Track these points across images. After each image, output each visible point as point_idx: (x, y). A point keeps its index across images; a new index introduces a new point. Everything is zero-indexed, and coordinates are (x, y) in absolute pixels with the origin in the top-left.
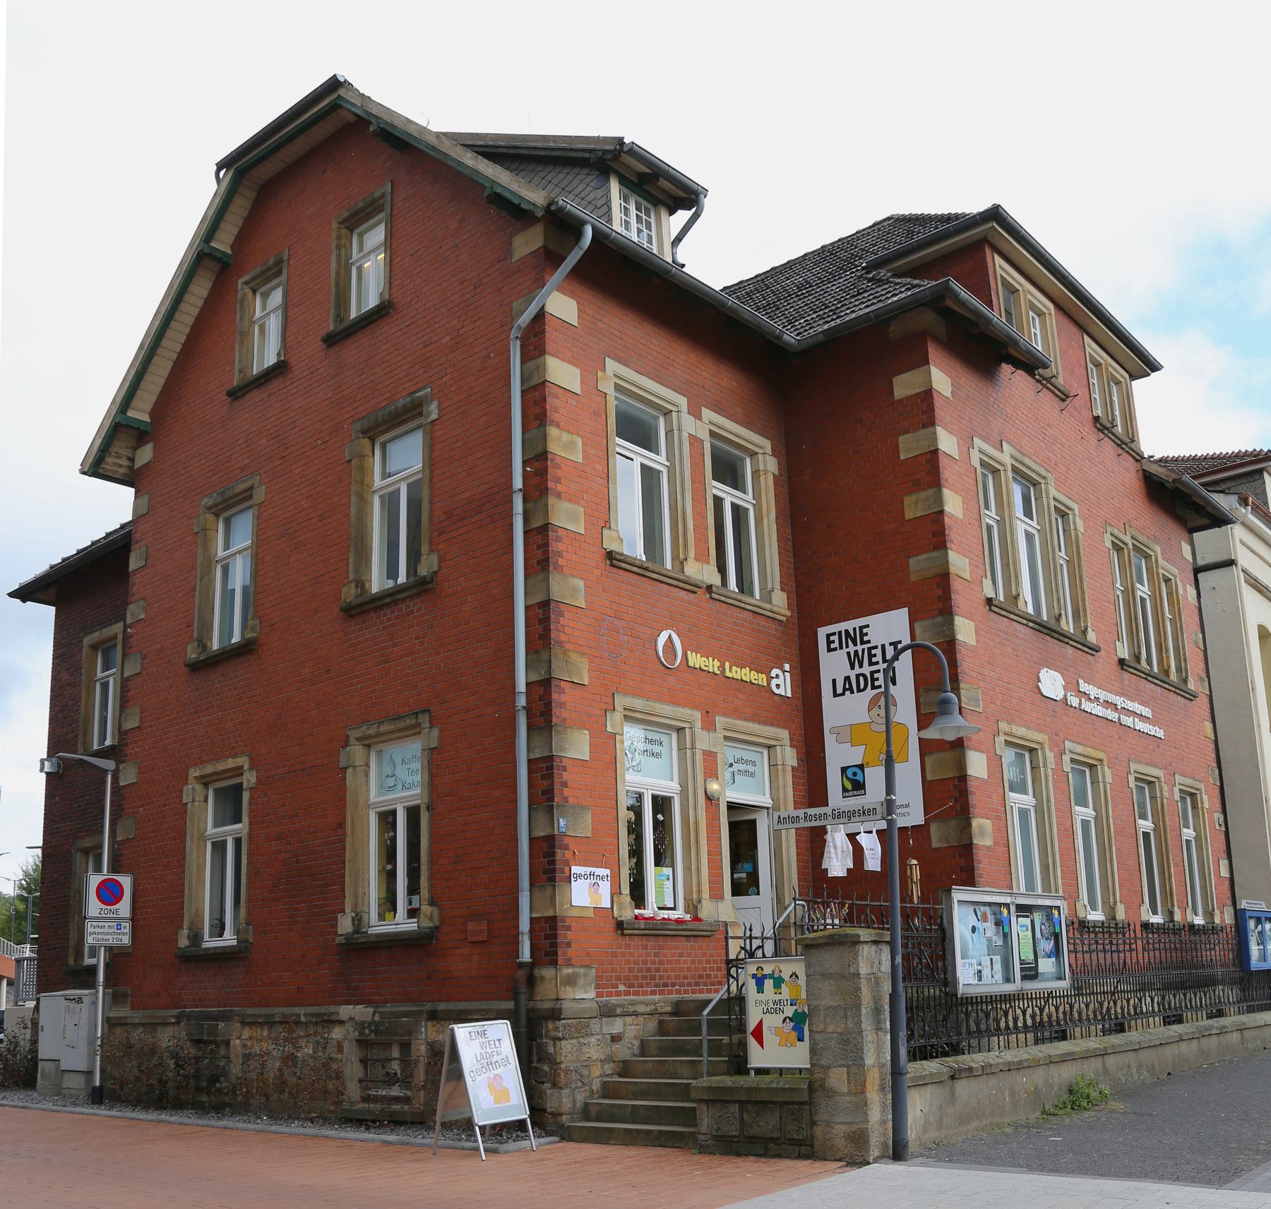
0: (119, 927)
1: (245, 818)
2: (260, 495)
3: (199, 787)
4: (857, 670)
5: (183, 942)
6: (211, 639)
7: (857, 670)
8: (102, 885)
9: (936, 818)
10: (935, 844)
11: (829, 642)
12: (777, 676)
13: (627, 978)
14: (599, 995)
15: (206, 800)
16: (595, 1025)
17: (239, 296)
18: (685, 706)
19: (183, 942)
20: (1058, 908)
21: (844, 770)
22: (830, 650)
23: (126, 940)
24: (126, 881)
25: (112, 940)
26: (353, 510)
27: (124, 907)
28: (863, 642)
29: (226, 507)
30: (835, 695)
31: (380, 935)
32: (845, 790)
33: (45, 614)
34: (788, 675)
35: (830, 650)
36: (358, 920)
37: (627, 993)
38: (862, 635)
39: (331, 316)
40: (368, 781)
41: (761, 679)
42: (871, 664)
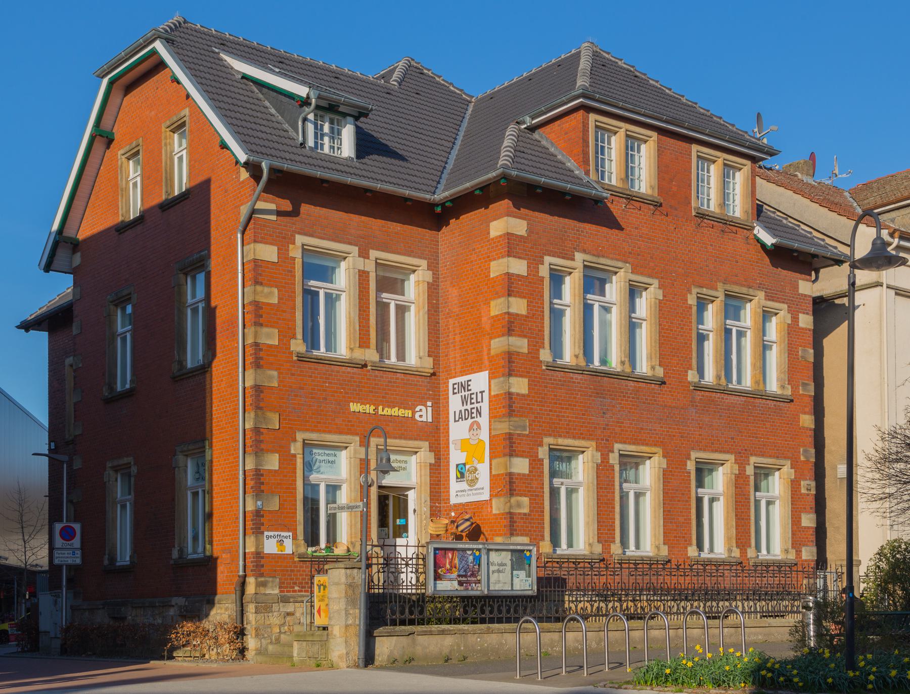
0: (74, 553)
1: (132, 493)
2: (135, 297)
3: (112, 473)
4: (465, 407)
5: (106, 562)
6: (116, 384)
7: (465, 407)
8: (63, 529)
9: (496, 496)
10: (494, 512)
11: (454, 389)
12: (421, 410)
13: (301, 583)
14: (281, 592)
15: (116, 480)
16: (275, 607)
17: (119, 163)
18: (347, 434)
19: (106, 562)
20: (530, 551)
21: (457, 465)
22: (454, 393)
23: (78, 561)
24: (77, 527)
25: (70, 561)
26: (176, 318)
27: (77, 542)
28: (468, 390)
29: (120, 302)
30: (455, 421)
31: (194, 559)
32: (457, 478)
33: (42, 338)
34: (430, 409)
35: (454, 393)
36: (181, 551)
37: (300, 591)
38: (469, 385)
39: (164, 191)
40: (186, 475)
41: (408, 413)
42: (471, 403)
